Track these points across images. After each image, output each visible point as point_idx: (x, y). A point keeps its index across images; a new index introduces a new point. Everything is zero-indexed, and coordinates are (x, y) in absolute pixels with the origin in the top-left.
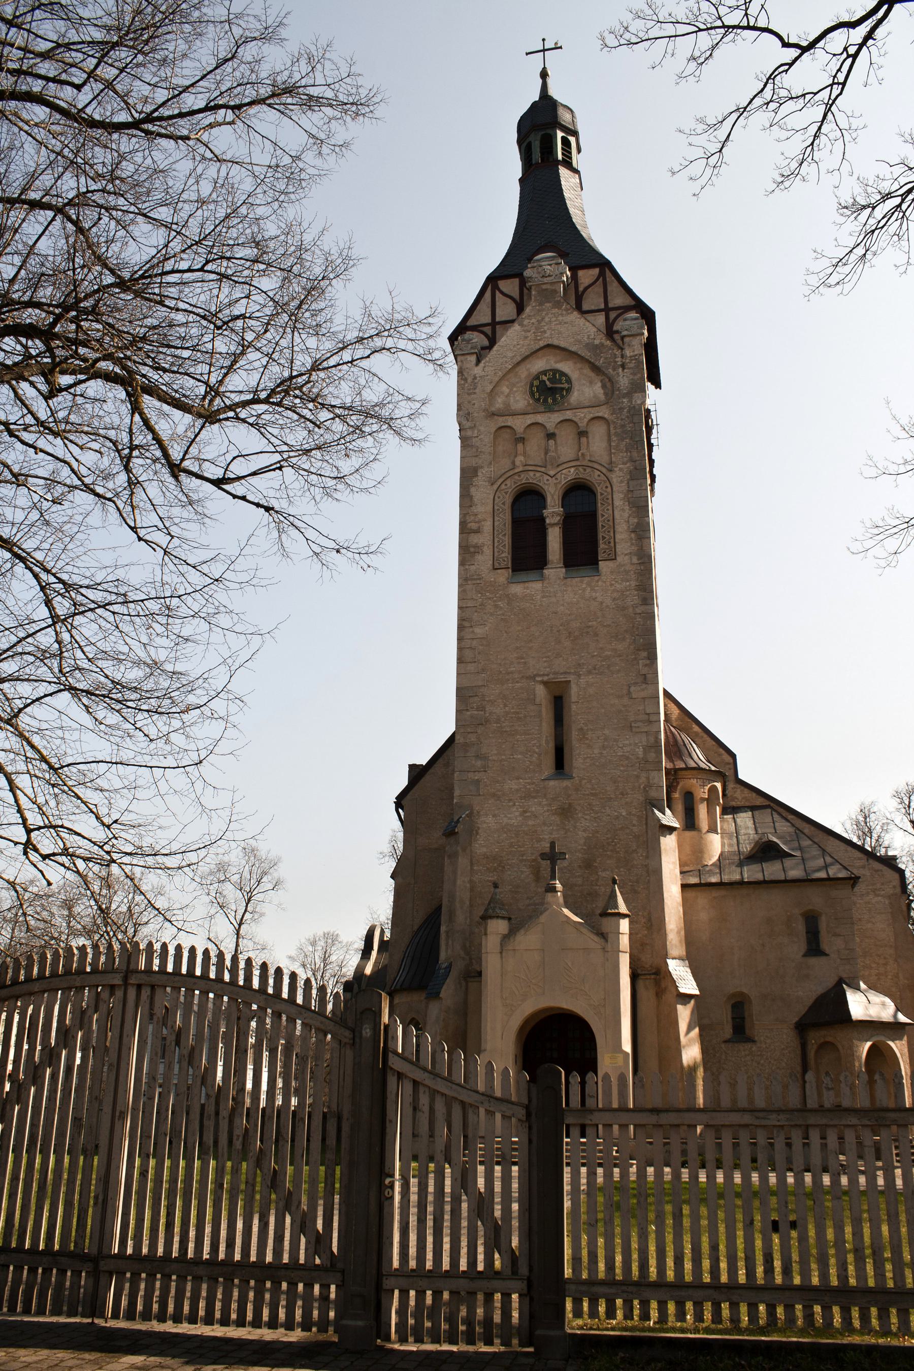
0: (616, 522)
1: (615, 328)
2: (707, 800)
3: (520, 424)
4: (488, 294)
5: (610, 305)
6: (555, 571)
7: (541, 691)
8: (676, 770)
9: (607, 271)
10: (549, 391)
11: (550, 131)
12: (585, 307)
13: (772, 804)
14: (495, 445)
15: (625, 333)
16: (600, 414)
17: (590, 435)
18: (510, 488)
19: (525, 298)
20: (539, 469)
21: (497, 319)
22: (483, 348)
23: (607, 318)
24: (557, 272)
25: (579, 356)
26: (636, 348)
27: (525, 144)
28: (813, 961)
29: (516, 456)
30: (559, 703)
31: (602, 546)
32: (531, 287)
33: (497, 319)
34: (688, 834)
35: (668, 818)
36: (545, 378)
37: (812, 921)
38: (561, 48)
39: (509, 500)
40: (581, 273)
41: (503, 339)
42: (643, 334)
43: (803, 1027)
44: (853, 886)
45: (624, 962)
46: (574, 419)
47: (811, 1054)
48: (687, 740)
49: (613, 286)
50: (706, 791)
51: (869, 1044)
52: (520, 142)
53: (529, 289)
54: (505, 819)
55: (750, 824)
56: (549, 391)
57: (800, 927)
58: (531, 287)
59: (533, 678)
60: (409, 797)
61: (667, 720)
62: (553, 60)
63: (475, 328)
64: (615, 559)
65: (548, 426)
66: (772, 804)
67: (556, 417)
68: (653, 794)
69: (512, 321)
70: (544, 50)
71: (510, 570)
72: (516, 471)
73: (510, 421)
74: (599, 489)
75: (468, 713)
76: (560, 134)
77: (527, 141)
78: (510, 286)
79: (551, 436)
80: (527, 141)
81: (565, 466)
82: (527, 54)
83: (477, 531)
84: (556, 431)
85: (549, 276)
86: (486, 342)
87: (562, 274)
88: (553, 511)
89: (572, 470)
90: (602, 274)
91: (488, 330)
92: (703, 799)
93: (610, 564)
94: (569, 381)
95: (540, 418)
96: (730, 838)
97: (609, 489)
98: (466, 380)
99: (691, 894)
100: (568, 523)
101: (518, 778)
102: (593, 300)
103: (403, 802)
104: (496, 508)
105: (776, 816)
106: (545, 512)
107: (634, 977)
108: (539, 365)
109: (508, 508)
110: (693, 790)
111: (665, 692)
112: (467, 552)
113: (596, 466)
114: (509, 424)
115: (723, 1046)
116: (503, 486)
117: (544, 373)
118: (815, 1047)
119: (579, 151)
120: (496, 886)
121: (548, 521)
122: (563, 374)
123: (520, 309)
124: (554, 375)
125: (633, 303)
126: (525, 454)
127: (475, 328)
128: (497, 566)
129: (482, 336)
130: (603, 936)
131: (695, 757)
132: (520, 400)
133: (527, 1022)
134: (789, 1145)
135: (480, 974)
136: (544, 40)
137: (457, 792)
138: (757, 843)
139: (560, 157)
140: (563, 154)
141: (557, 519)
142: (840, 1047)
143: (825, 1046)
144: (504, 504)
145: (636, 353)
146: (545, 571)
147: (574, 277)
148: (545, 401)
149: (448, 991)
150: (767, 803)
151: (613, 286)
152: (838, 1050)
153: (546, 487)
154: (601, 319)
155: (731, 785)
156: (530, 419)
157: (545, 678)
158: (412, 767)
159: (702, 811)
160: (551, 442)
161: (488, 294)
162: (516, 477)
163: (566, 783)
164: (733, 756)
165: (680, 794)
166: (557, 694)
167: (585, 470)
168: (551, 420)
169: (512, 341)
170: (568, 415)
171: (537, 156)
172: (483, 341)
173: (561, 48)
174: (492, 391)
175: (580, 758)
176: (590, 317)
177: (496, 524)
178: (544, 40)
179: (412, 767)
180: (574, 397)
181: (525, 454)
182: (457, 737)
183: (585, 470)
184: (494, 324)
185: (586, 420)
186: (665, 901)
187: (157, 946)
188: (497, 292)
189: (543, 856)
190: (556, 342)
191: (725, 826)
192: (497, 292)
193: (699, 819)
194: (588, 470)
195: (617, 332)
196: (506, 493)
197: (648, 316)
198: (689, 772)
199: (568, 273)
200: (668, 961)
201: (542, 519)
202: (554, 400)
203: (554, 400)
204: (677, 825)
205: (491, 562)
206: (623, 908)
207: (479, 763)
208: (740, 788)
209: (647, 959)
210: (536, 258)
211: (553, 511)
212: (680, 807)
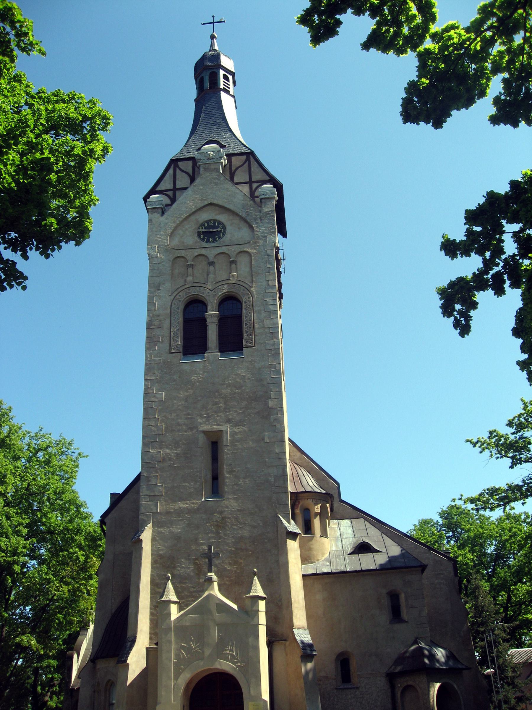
1: (256, 194)
2: (320, 514)
3: (190, 255)
4: (171, 171)
5: (253, 180)
6: (213, 354)
7: (202, 439)
9: (251, 158)
10: (211, 232)
12: (236, 180)
14: (173, 268)
15: (263, 197)
17: (238, 264)
18: (183, 297)
19: (196, 173)
21: (177, 187)
22: (167, 205)
23: (251, 188)
24: (218, 157)
26: (271, 207)
27: (199, 78)
29: (187, 277)
32: (200, 165)
33: (177, 187)
35: (292, 527)
37: (394, 597)
38: (224, 22)
39: (182, 307)
41: (180, 199)
42: (275, 197)
44: (423, 571)
45: (262, 631)
47: (398, 694)
49: (255, 167)
50: (319, 507)
51: (438, 685)
52: (196, 77)
53: (199, 168)
55: (350, 530)
56: (211, 232)
57: (386, 602)
58: (200, 165)
60: (110, 516)
63: (160, 192)
65: (209, 256)
69: (186, 188)
70: (213, 23)
71: (182, 354)
72: (187, 286)
73: (183, 253)
74: (244, 299)
76: (222, 72)
77: (201, 76)
79: (212, 264)
80: (201, 76)
81: (221, 283)
82: (202, 24)
83: (159, 327)
84: (215, 261)
85: (213, 159)
86: (168, 202)
87: (221, 157)
88: (212, 313)
90: (248, 160)
92: (316, 514)
94: (224, 228)
100: (222, 321)
102: (241, 176)
103: (106, 520)
104: (173, 311)
105: (368, 524)
107: (270, 644)
108: (205, 216)
110: (310, 508)
111: (290, 440)
112: (151, 341)
114: (183, 255)
115: (335, 691)
116: (178, 297)
118: (401, 689)
119: (235, 84)
121: (208, 320)
122: (220, 223)
123: (192, 179)
124: (214, 223)
125: (268, 178)
126: (193, 275)
128: (173, 351)
129: (166, 197)
132: (191, 239)
136: (213, 16)
139: (222, 87)
142: (419, 690)
143: (406, 688)
144: (178, 308)
151: (255, 167)
152: (417, 692)
153: (207, 298)
154: (246, 189)
155: (336, 505)
156: (197, 252)
158: (113, 495)
159: (317, 523)
160: (212, 268)
161: (171, 171)
164: (338, 484)
165: (300, 510)
166: (214, 440)
167: (234, 286)
169: (188, 201)
170: (223, 249)
171: (207, 85)
172: (166, 200)
173: (224, 22)
176: (239, 186)
177: (173, 322)
178: (213, 16)
179: (113, 495)
180: (227, 238)
181: (193, 275)
184: (174, 189)
186: (291, 586)
188: (177, 169)
190: (215, 202)
192: (177, 169)
193: (314, 527)
195: (257, 197)
196: (180, 301)
197: (279, 187)
199: (225, 157)
200: (294, 630)
201: (204, 320)
204: (298, 531)
205: (168, 348)
211: (212, 313)
212: (300, 518)
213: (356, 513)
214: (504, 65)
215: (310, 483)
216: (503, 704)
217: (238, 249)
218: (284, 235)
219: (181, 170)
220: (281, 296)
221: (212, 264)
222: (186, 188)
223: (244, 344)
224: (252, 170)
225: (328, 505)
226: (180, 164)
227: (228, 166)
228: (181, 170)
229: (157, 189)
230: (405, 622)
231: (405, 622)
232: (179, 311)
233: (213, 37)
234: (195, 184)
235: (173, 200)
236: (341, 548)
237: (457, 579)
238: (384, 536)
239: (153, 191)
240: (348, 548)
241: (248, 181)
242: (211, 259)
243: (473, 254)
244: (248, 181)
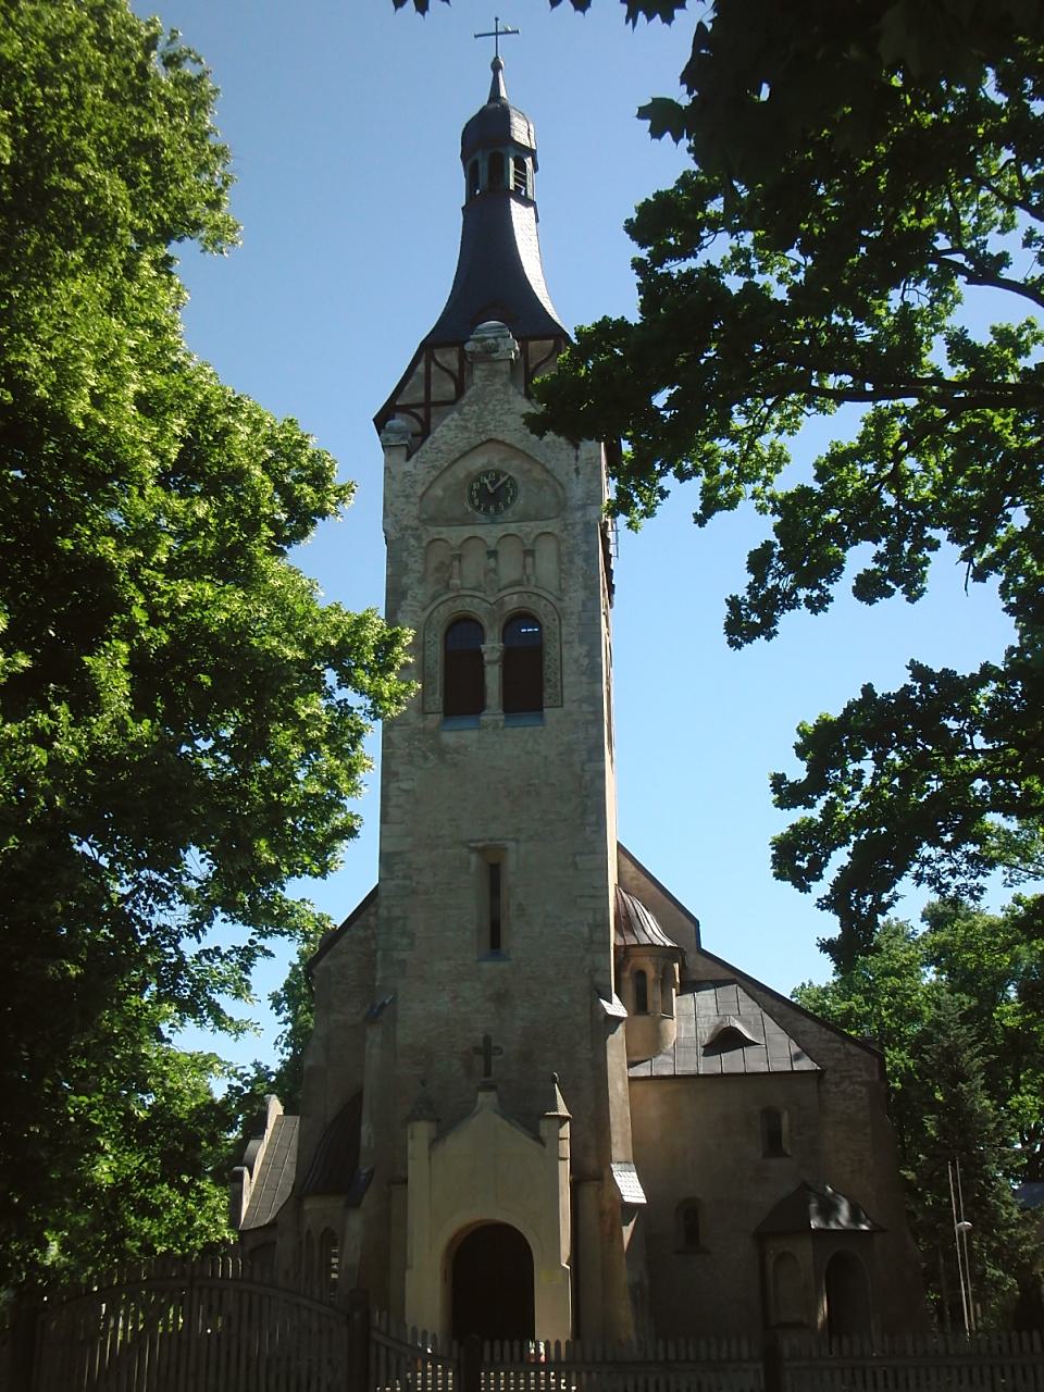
0: (564, 661)
4: (421, 368)
8: (627, 948)
11: (501, 150)
13: (738, 978)
16: (549, 530)
17: (537, 555)
20: (477, 594)
21: (433, 399)
25: (524, 453)
28: (774, 1162)
30: (494, 873)
31: (548, 691)
33: (433, 399)
34: (641, 1019)
35: (615, 1008)
36: (486, 481)
39: (441, 632)
40: (532, 344)
41: (439, 429)
43: (761, 1237)
45: (564, 1169)
46: (519, 534)
47: (770, 1262)
48: (640, 908)
52: (464, 157)
54: (438, 1003)
59: (465, 844)
61: (620, 883)
62: (507, 49)
63: (405, 409)
64: (562, 706)
66: (738, 978)
67: (497, 531)
68: (598, 978)
75: (393, 883)
78: (450, 358)
82: (476, 36)
84: (499, 548)
86: (418, 427)
88: (492, 648)
89: (515, 597)
91: (420, 412)
93: (557, 712)
95: (479, 531)
96: (688, 1022)
97: (557, 622)
98: (393, 478)
99: (639, 1087)
100: (509, 659)
101: (448, 959)
106: (483, 648)
107: (575, 1186)
108: (478, 462)
109: (439, 639)
111: (619, 846)
113: (544, 594)
117: (486, 474)
119: (536, 168)
120: (423, 1083)
121: (486, 657)
127: (405, 409)
129: (415, 420)
130: (539, 1139)
131: (649, 932)
133: (452, 1241)
134: (918, 1378)
135: (406, 1181)
136: (497, 19)
137: (379, 975)
138: (717, 1027)
139: (512, 188)
140: (516, 180)
141: (496, 655)
145: (592, 455)
146: (483, 718)
147: (524, 350)
148: (486, 510)
149: (369, 1199)
150: (733, 977)
157: (480, 845)
161: (421, 368)
162: (450, 603)
163: (503, 965)
164: (696, 923)
165: (631, 973)
167: (529, 597)
168: (491, 533)
169: (447, 432)
170: (512, 528)
171: (483, 179)
174: (424, 494)
175: (516, 939)
178: (497, 19)
182: (383, 894)
183: (529, 597)
184: (427, 404)
185: (533, 536)
187: (420, 1330)
188: (433, 364)
189: (477, 1050)
191: (683, 1006)
194: (534, 598)
198: (641, 949)
200: (613, 1166)
202: (497, 509)
203: (497, 509)
206: (563, 1111)
207: (405, 941)
208: (702, 959)
209: (591, 1164)
210: (480, 327)
211: (492, 648)
212: (629, 988)
213: (726, 976)
215: (652, 931)
219: (438, 364)
220: (611, 588)
221: (493, 554)
223: (547, 702)
225: (677, 966)
227: (522, 360)
228: (438, 364)
230: (787, 1156)
231: (787, 1156)
232: (438, 639)
233: (496, 67)
236: (694, 1035)
238: (766, 1016)
240: (705, 1034)
242: (491, 542)
243: (1033, 368)
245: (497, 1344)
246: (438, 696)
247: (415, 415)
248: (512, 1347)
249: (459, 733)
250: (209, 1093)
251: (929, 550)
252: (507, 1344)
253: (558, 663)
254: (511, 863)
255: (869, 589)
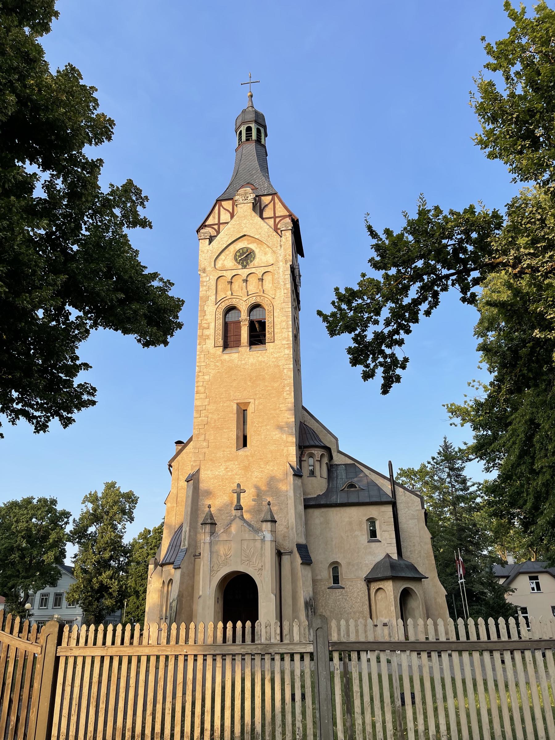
21: (221, 222)
33: (221, 222)
69: (227, 223)
89: (254, 298)
90: (273, 199)
91: (216, 227)
95: (240, 272)
116: (220, 306)
118: (375, 590)
123: (232, 216)
142: (387, 592)
154: (271, 222)
156: (234, 272)
180: (256, 262)
184: (219, 224)
214: (281, 486)
216: (469, 491)
217: (263, 270)
218: (302, 255)
222: (227, 223)
224: (225, 246)
226: (223, 203)
229: (207, 224)
234: (233, 220)
235: (218, 232)
237: (424, 511)
239: (203, 226)
241: (273, 216)
244: (273, 216)
245: (239, 624)
246: (221, 340)
247: (213, 228)
248: (96, 631)
249: (230, 355)
250: (121, 537)
251: (386, 347)
252: (119, 627)
253: (272, 324)
254: (250, 410)
255: (488, 90)
